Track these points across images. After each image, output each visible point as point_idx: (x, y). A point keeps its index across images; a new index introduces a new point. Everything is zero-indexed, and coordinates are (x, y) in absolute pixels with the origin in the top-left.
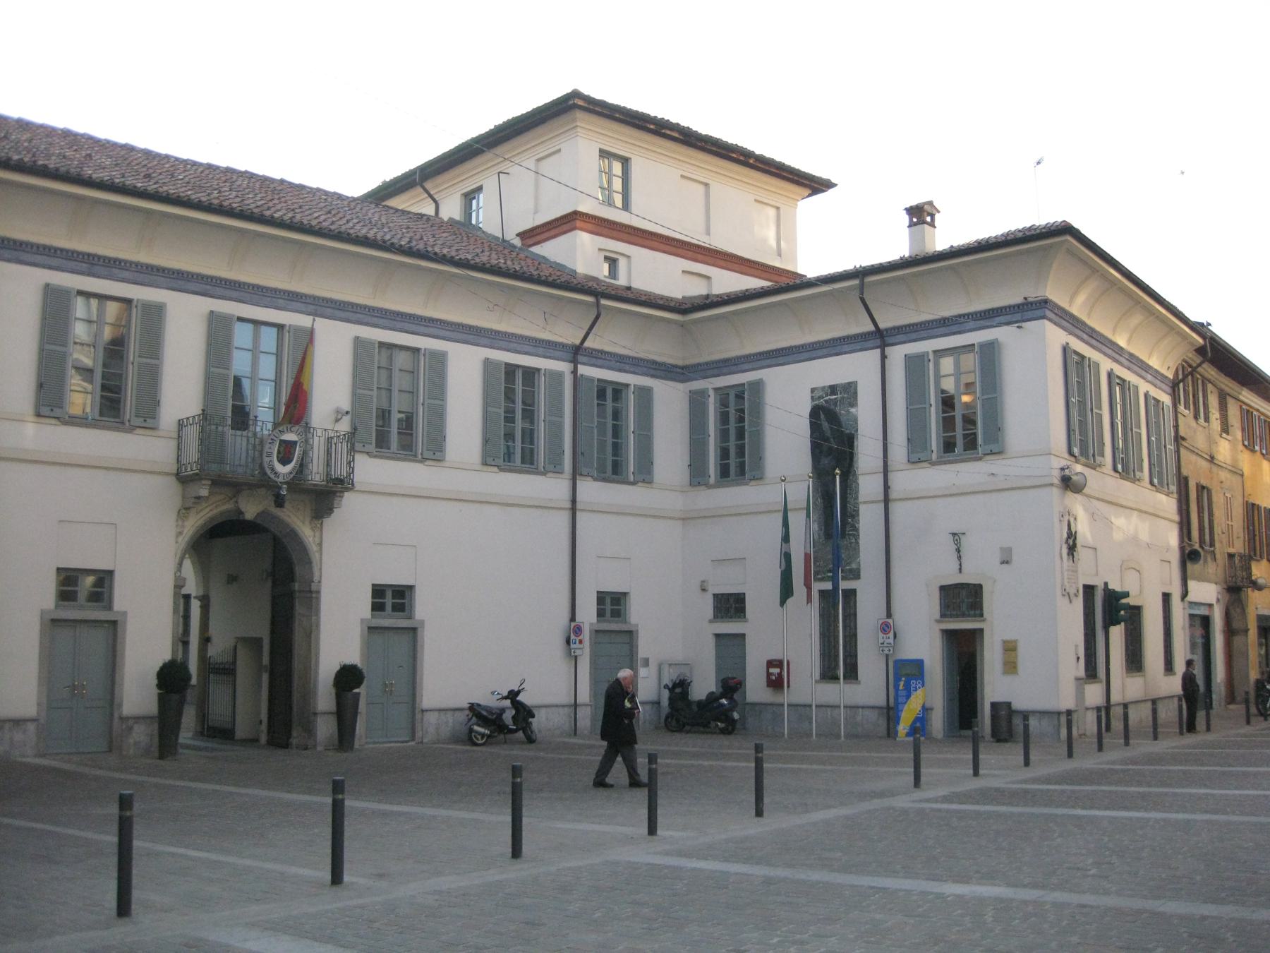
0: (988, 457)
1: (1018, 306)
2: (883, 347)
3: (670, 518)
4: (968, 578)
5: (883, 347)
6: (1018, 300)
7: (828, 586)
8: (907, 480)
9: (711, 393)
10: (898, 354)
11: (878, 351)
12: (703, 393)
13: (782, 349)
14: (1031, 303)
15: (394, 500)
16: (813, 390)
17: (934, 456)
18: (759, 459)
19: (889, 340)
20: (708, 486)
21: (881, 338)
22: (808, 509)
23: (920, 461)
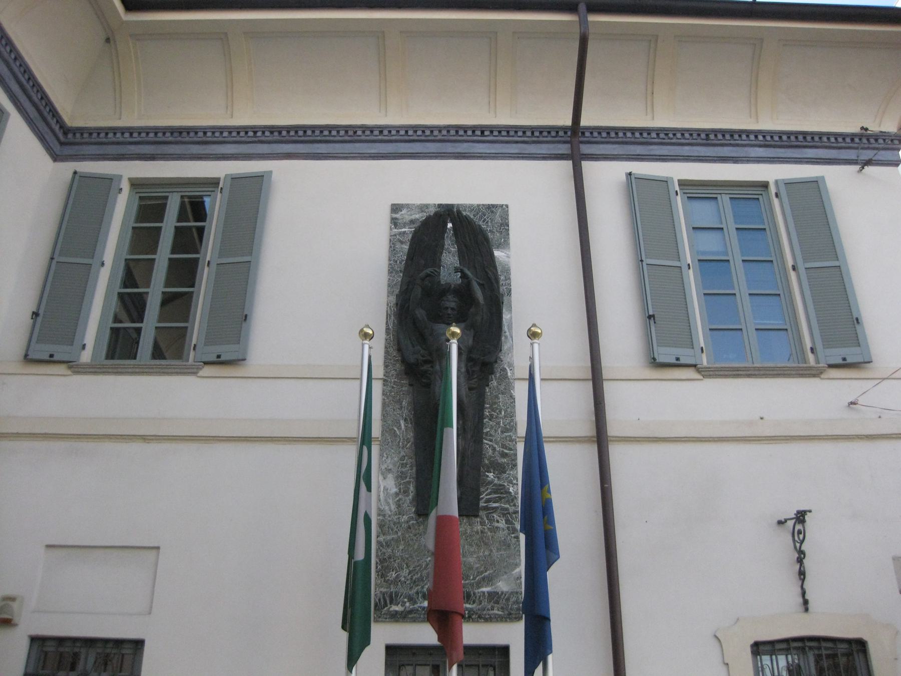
0: (207, 371)
1: (853, 136)
2: (576, 159)
3: (17, 436)
4: (828, 621)
5: (576, 159)
6: (852, 128)
7: (424, 634)
8: (637, 400)
9: (125, 186)
10: (606, 177)
11: (568, 165)
12: (108, 183)
13: (304, 128)
14: (868, 138)
15: (770, 332)
16: (396, 208)
17: (86, 357)
18: (235, 319)
19: (586, 149)
20: (74, 367)
21: (574, 143)
22: (366, 439)
23: (51, 360)
